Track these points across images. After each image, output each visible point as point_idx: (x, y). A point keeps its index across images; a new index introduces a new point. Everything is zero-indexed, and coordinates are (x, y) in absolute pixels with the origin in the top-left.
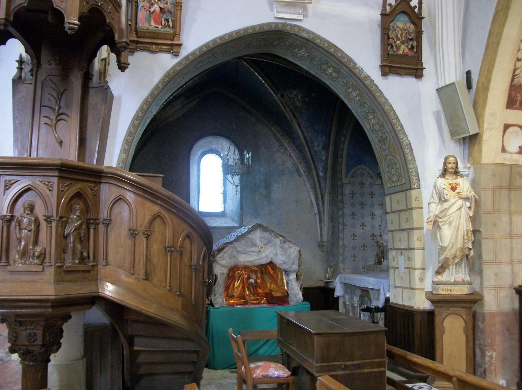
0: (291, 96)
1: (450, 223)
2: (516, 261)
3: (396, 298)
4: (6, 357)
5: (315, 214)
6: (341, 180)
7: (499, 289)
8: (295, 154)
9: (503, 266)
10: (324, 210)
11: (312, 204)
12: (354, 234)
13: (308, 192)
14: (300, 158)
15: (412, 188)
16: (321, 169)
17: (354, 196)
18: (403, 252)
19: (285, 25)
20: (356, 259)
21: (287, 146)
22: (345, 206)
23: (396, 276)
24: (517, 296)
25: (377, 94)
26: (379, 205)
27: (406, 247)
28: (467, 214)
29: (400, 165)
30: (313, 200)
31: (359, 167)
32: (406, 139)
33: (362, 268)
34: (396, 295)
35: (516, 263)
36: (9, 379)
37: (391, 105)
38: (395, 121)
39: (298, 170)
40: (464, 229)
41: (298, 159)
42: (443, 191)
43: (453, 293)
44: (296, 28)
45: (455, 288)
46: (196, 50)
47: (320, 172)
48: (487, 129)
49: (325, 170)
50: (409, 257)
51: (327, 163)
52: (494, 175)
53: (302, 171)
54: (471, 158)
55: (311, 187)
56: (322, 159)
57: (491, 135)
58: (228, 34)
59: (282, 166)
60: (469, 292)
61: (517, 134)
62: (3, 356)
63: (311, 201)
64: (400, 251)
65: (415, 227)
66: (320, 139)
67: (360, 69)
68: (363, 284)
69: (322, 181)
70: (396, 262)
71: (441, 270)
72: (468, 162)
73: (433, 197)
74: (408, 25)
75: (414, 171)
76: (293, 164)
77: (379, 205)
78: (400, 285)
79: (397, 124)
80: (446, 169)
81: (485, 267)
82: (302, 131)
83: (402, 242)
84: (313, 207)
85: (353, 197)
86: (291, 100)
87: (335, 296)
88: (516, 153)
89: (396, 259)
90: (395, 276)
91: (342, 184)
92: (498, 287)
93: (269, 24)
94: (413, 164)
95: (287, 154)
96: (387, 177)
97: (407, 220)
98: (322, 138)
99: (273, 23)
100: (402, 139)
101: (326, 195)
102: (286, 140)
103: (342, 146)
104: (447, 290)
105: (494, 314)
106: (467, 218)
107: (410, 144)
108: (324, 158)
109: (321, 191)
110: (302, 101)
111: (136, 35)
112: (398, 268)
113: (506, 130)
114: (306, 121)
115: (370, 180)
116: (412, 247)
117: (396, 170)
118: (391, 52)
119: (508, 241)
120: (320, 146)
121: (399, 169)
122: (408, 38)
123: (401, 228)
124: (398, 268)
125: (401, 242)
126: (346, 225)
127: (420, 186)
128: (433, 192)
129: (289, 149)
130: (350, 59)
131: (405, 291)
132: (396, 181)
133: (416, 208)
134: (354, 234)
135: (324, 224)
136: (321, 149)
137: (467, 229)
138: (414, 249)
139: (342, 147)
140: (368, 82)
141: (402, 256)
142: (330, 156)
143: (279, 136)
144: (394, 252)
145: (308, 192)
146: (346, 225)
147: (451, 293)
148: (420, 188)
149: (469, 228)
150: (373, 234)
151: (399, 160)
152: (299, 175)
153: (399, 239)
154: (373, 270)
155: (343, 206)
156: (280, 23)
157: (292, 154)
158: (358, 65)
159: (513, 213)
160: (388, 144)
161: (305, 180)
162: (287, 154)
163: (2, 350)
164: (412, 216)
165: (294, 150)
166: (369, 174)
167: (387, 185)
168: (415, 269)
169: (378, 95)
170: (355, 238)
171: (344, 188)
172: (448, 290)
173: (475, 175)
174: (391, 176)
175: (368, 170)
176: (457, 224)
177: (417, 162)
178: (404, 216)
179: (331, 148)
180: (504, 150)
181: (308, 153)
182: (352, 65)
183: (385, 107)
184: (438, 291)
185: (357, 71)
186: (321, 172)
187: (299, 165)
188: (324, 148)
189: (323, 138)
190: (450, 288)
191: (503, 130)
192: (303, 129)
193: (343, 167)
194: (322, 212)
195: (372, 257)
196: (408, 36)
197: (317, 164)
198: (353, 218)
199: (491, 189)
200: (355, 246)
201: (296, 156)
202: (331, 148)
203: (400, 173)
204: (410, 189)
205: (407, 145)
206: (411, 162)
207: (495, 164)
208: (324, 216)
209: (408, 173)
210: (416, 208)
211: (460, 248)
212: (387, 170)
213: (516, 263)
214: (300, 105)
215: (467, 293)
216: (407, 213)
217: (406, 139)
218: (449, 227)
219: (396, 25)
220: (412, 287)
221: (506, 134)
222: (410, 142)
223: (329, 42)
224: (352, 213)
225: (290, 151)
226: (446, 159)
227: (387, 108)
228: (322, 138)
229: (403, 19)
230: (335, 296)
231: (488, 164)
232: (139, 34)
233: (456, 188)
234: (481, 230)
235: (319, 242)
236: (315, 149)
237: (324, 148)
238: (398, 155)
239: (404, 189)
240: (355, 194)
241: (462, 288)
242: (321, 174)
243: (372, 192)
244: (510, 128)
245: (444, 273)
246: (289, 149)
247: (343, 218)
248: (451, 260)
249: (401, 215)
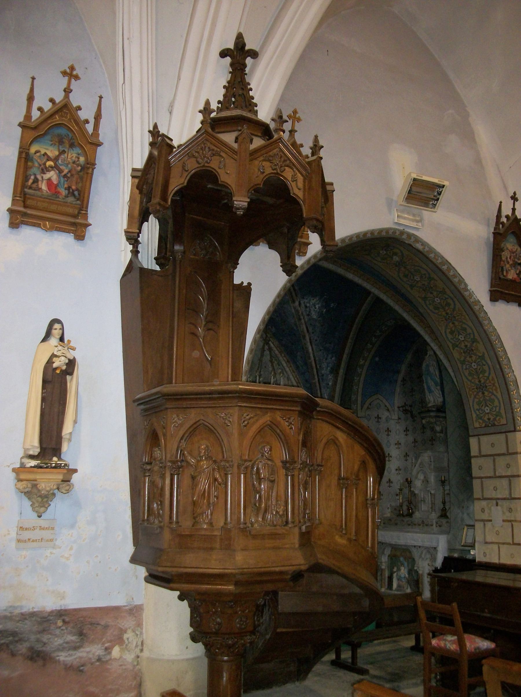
4: (105, 655)
8: (295, 376)
15: (517, 430)
18: (500, 502)
19: (402, 233)
21: (285, 365)
23: (487, 530)
25: (484, 322)
26: (396, 444)
31: (375, 397)
36: (110, 687)
37: (499, 336)
38: (501, 354)
44: (412, 237)
46: (318, 252)
51: (334, 391)
56: (328, 384)
58: (348, 236)
62: (101, 654)
64: (494, 502)
66: (330, 360)
67: (471, 291)
74: (516, 248)
77: (396, 444)
78: (494, 540)
79: (503, 357)
83: (498, 491)
89: (487, 511)
90: (485, 531)
93: (387, 230)
99: (391, 229)
100: (508, 374)
103: (359, 370)
107: (516, 381)
110: (319, 312)
111: (22, 204)
114: (318, 337)
115: (387, 414)
118: (502, 277)
120: (329, 368)
122: (516, 262)
124: (491, 521)
129: (287, 369)
130: (462, 280)
136: (328, 373)
139: (359, 372)
140: (477, 308)
141: (499, 507)
144: (484, 503)
150: (390, 480)
154: (396, 524)
156: (399, 230)
157: (291, 377)
158: (469, 288)
160: (486, 378)
163: (100, 646)
165: (293, 372)
166: (386, 406)
169: (486, 322)
175: (384, 401)
178: (501, 462)
179: (341, 372)
182: (462, 286)
183: (492, 337)
185: (466, 294)
188: (331, 372)
189: (333, 359)
195: (388, 508)
196: (516, 260)
202: (341, 372)
203: (499, 412)
204: (515, 430)
205: (512, 382)
206: (516, 401)
209: (512, 413)
212: (476, 407)
214: (315, 317)
216: (508, 458)
219: (506, 246)
222: (516, 379)
223: (443, 257)
225: (289, 372)
227: (493, 338)
228: (331, 358)
229: (512, 240)
232: (29, 202)
237: (331, 372)
243: (388, 429)
246: (287, 369)
249: (496, 461)
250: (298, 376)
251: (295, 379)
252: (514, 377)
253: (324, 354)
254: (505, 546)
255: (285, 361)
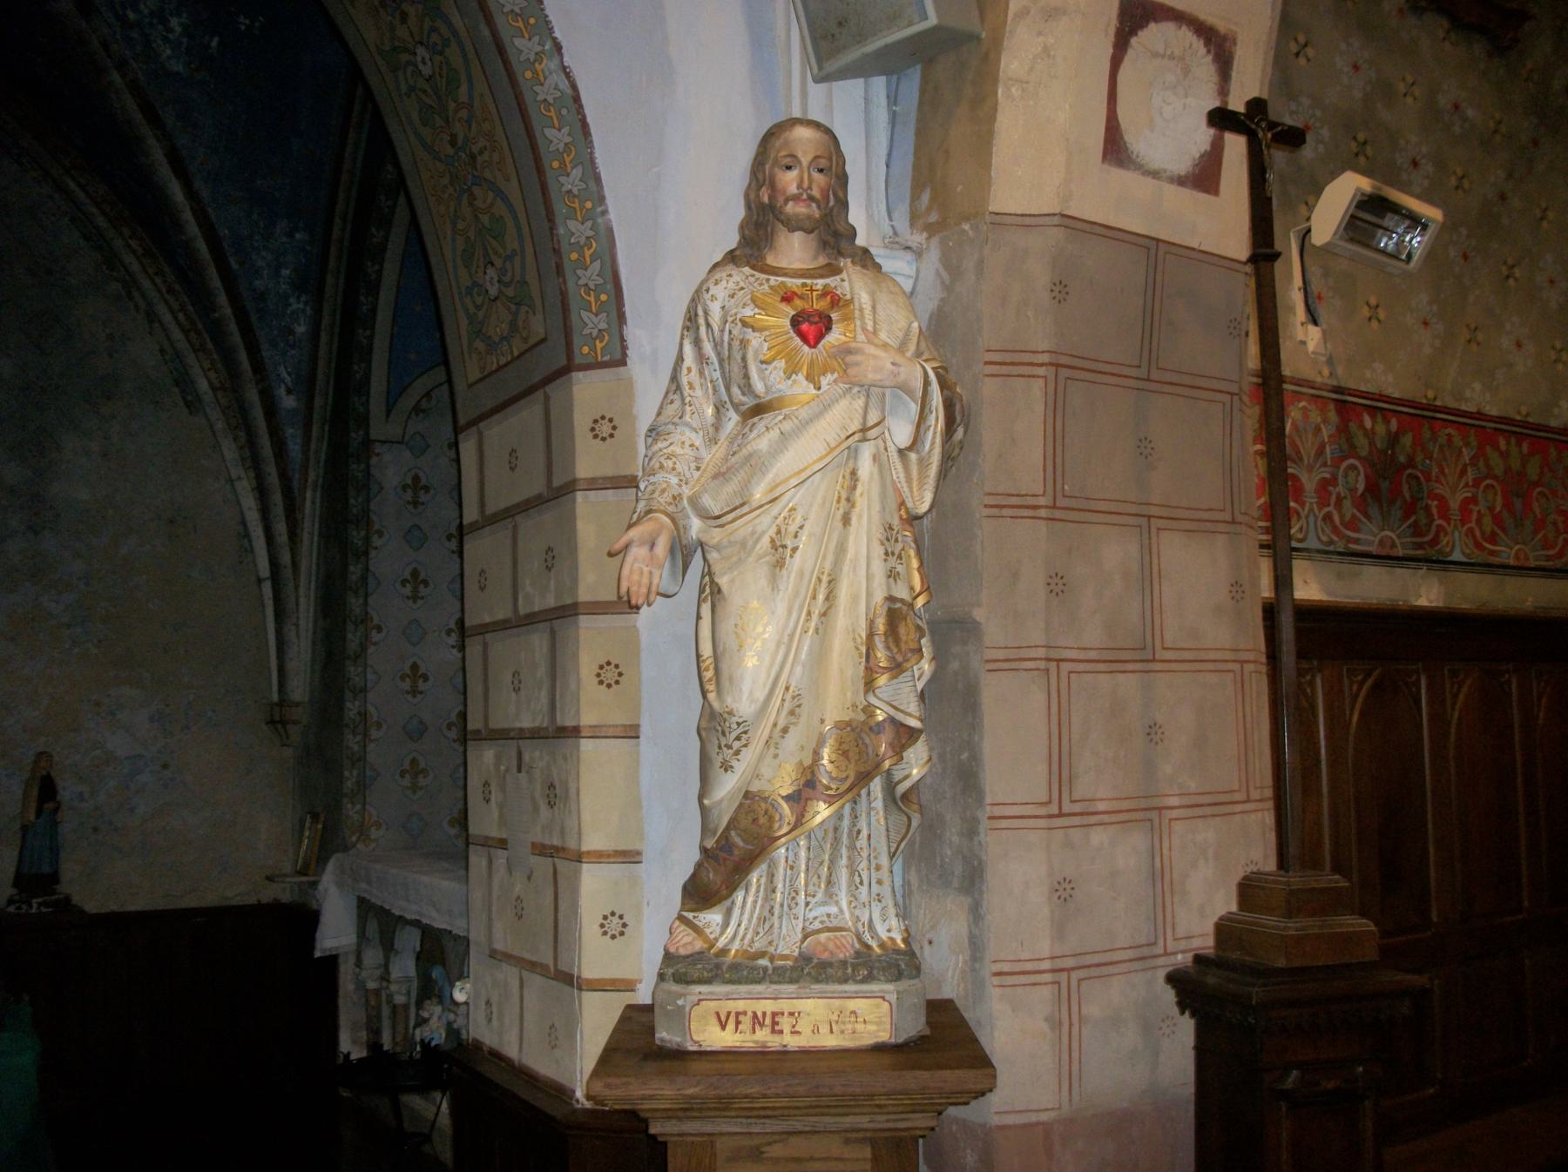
0: (132, 16)
1: (780, 552)
2: (1174, 801)
3: (495, 1023)
5: (260, 581)
6: (364, 421)
7: (1075, 976)
9: (1098, 837)
10: (295, 565)
11: (246, 535)
12: (415, 667)
13: (231, 481)
14: (200, 326)
16: (288, 379)
17: (423, 497)
20: (422, 781)
21: (135, 267)
22: (376, 541)
24: (1185, 1029)
27: (540, 721)
28: (892, 504)
29: (520, 237)
30: (253, 517)
32: (554, 64)
33: (451, 823)
34: (494, 1000)
35: (1175, 813)
39: (184, 382)
40: (869, 595)
41: (186, 332)
42: (744, 344)
43: (792, 1042)
45: (807, 1005)
47: (282, 391)
48: (1023, 13)
49: (306, 385)
50: (552, 786)
52: (1060, 290)
53: (203, 385)
54: (926, 198)
55: (243, 459)
56: (292, 332)
57: (1046, 50)
59: (111, 356)
60: (895, 1027)
61: (1186, 72)
63: (244, 523)
65: (584, 595)
68: (414, 908)
69: (290, 431)
70: (496, 814)
71: (712, 876)
72: (914, 218)
73: (679, 388)
75: (594, 258)
76: (162, 351)
80: (762, 208)
81: (992, 843)
82: (191, 194)
83: (523, 693)
84: (252, 551)
85: (415, 504)
86: (135, 35)
87: (318, 954)
88: (1181, 181)
91: (367, 443)
92: (1070, 963)
94: (588, 216)
95: (137, 308)
96: (464, 322)
97: (550, 559)
98: (290, 235)
101: (309, 494)
102: (133, 243)
104: (746, 1021)
105: (1047, 1128)
106: (896, 522)
107: (577, 99)
108: (301, 329)
109: (284, 476)
112: (503, 844)
113: (1133, 32)
116: (569, 723)
117: (502, 271)
119: (1128, 684)
120: (286, 272)
121: (517, 259)
123: (523, 610)
124: (503, 844)
125: (517, 690)
126: (379, 629)
127: (624, 348)
128: (680, 358)
129: (146, 284)
131: (535, 981)
132: (503, 338)
133: (595, 484)
134: (415, 667)
135: (297, 625)
137: (891, 599)
138: (575, 732)
142: (326, 321)
143: (101, 221)
145: (231, 481)
146: (379, 629)
147: (774, 1042)
148: (622, 362)
149: (902, 592)
151: (519, 208)
152: (188, 405)
153: (509, 677)
155: (367, 539)
157: (161, 309)
159: (1161, 523)
161: (220, 425)
162: (137, 308)
164: (575, 526)
165: (170, 291)
167: (468, 369)
168: (579, 857)
170: (421, 685)
171: (374, 460)
172: (757, 1021)
173: (948, 288)
174: (481, 314)
176: (828, 566)
177: (610, 201)
180: (1115, 148)
181: (222, 299)
184: (685, 1030)
186: (289, 392)
187: (191, 359)
190: (769, 1006)
191: (1112, 31)
192: (198, 184)
193: (374, 364)
194: (288, 573)
197: (266, 352)
198: (415, 597)
199: (1041, 371)
200: (421, 722)
201: (181, 316)
207: (1070, 223)
208: (297, 587)
209: (559, 269)
210: (595, 484)
211: (840, 726)
213: (1175, 813)
214: (177, 67)
215: (884, 1036)
217: (554, 64)
218: (774, 581)
220: (563, 967)
221: (1131, 55)
222: (574, 87)
224: (407, 575)
226: (770, 137)
228: (290, 235)
230: (318, 954)
231: (1027, 222)
233: (826, 325)
234: (979, 614)
235: (272, 705)
236: (257, 283)
238: (515, 182)
239: (536, 379)
240: (427, 489)
241: (853, 1004)
242: (288, 402)
244: (1152, 26)
245: (739, 896)
246: (146, 284)
247: (366, 596)
248: (785, 808)
250: (190, 308)
251: (176, 318)
252: (564, 85)
253: (255, 217)
254: (1178, 822)
255: (134, 252)
